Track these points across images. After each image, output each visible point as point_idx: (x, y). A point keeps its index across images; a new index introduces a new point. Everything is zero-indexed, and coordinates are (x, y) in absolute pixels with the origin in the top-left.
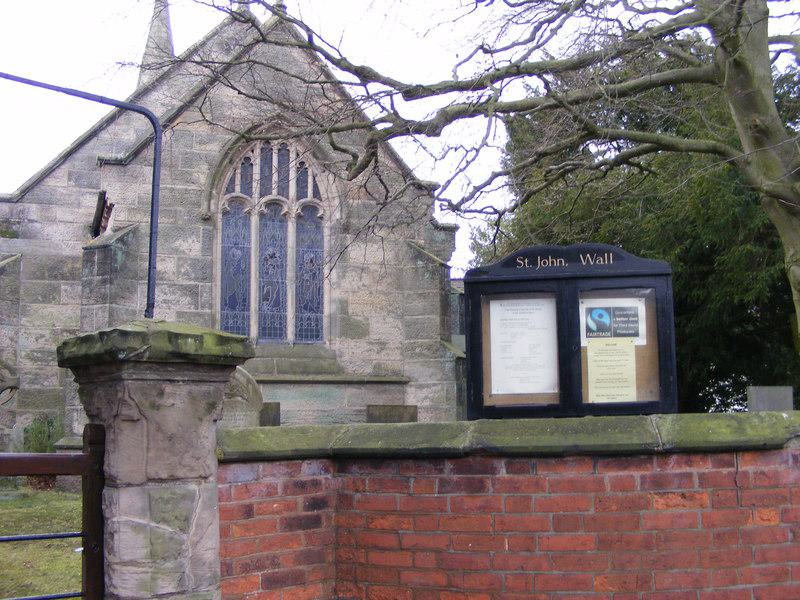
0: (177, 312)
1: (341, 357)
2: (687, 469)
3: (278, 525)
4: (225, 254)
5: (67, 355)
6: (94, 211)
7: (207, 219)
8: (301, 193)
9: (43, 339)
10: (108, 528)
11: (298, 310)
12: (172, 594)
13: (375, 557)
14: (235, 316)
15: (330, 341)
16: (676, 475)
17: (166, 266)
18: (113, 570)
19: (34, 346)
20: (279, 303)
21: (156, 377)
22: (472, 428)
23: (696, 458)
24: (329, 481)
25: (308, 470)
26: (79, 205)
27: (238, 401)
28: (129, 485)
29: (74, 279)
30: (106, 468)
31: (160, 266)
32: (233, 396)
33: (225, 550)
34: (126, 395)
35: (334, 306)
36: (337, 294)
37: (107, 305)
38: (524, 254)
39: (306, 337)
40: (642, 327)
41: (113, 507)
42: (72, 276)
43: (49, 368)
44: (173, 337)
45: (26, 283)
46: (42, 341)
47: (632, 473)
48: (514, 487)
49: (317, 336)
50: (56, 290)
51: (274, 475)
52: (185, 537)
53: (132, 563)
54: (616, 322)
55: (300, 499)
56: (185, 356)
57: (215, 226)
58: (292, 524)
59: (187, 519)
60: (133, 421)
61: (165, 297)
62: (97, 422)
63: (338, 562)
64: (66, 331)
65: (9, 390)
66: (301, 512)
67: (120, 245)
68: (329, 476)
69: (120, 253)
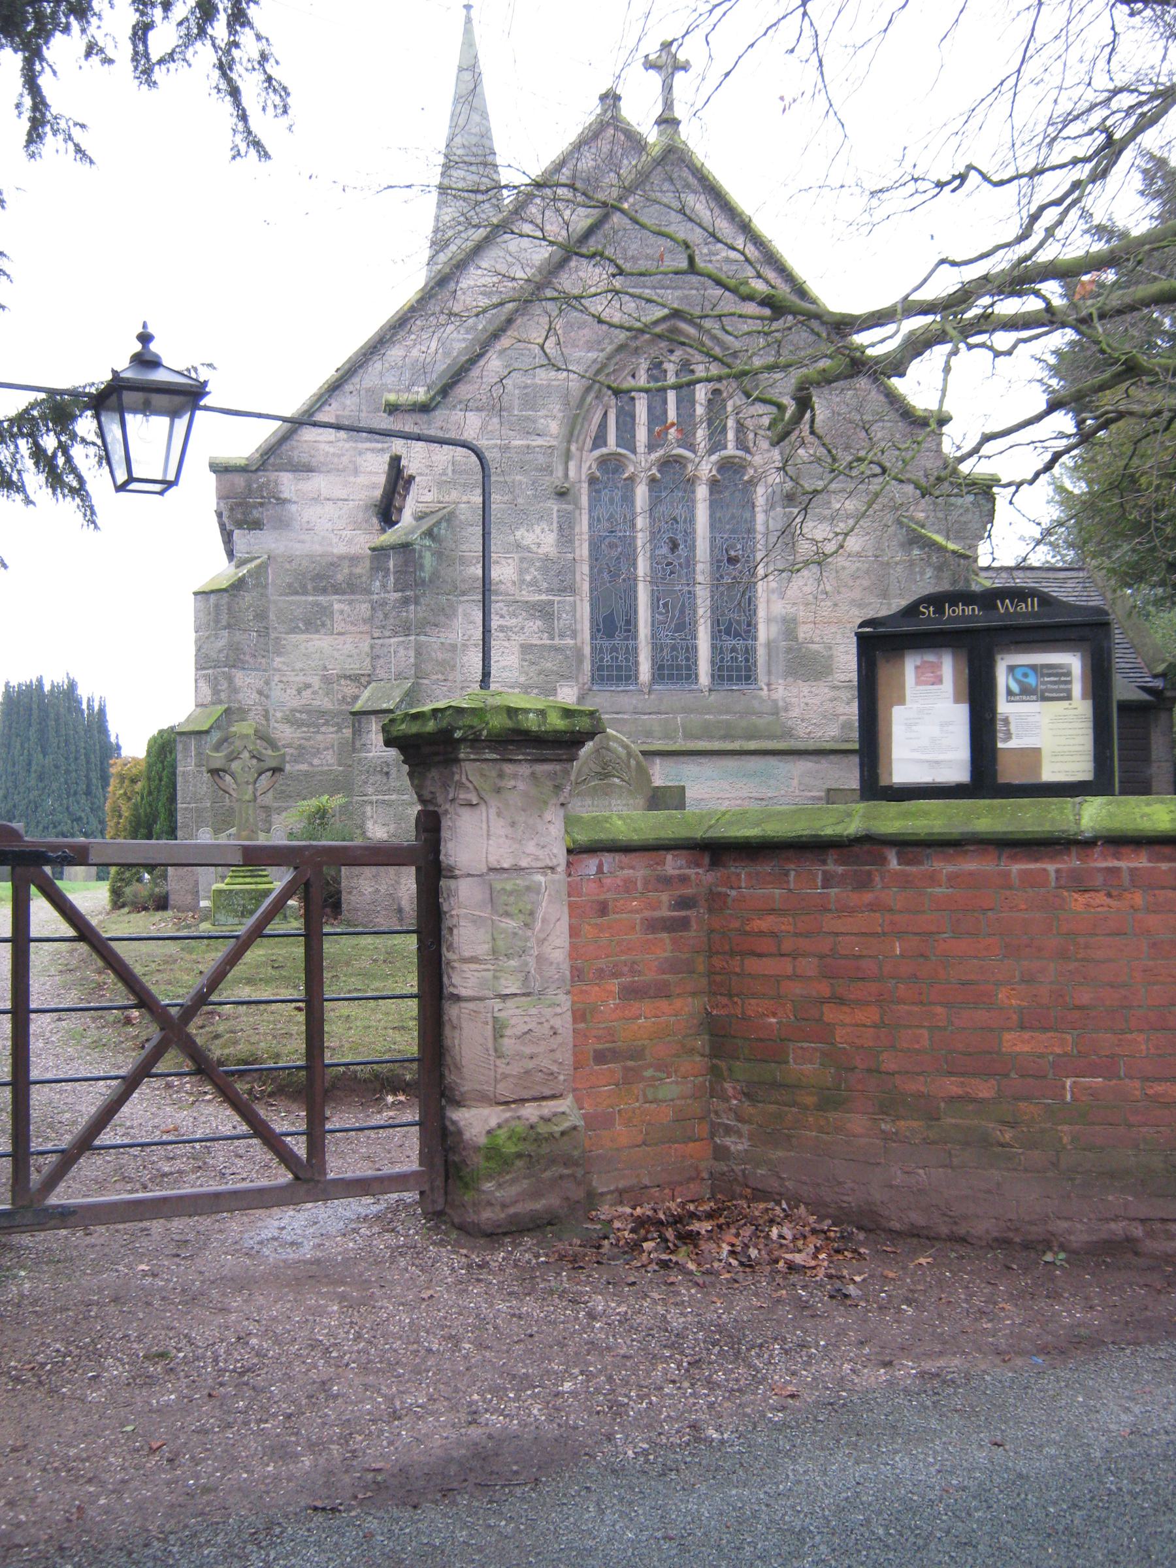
0: (522, 646)
1: (786, 710)
2: (1116, 864)
3: (638, 928)
4: (594, 547)
5: (395, 734)
6: (382, 479)
7: (562, 494)
8: (716, 445)
9: (309, 691)
10: (447, 922)
11: (715, 636)
12: (515, 995)
13: (754, 965)
14: (614, 649)
15: (769, 685)
16: (1100, 870)
17: (503, 572)
18: (453, 968)
19: (296, 703)
20: (685, 626)
21: (495, 756)
22: (861, 811)
23: (1125, 850)
24: (702, 877)
25: (672, 864)
26: (356, 472)
27: (614, 784)
28: (469, 875)
29: (353, 593)
30: (442, 857)
31: (495, 573)
32: (607, 776)
33: (574, 952)
34: (464, 777)
35: (774, 629)
36: (779, 608)
37: (412, 638)
38: (929, 600)
39: (730, 678)
40: (1077, 688)
41: (452, 899)
42: (351, 588)
43: (320, 737)
44: (512, 712)
45: (278, 601)
46: (307, 693)
47: (1044, 866)
48: (905, 882)
49: (748, 678)
50: (326, 611)
51: (633, 868)
52: (529, 933)
53: (473, 960)
54: (1043, 683)
55: (665, 897)
56: (527, 732)
57: (578, 507)
58: (654, 926)
59: (532, 913)
60: (472, 805)
61: (502, 622)
62: (431, 808)
63: (711, 972)
64: (346, 677)
65: (269, 774)
66: (665, 912)
67: (427, 542)
68: (700, 871)
69: (428, 554)
